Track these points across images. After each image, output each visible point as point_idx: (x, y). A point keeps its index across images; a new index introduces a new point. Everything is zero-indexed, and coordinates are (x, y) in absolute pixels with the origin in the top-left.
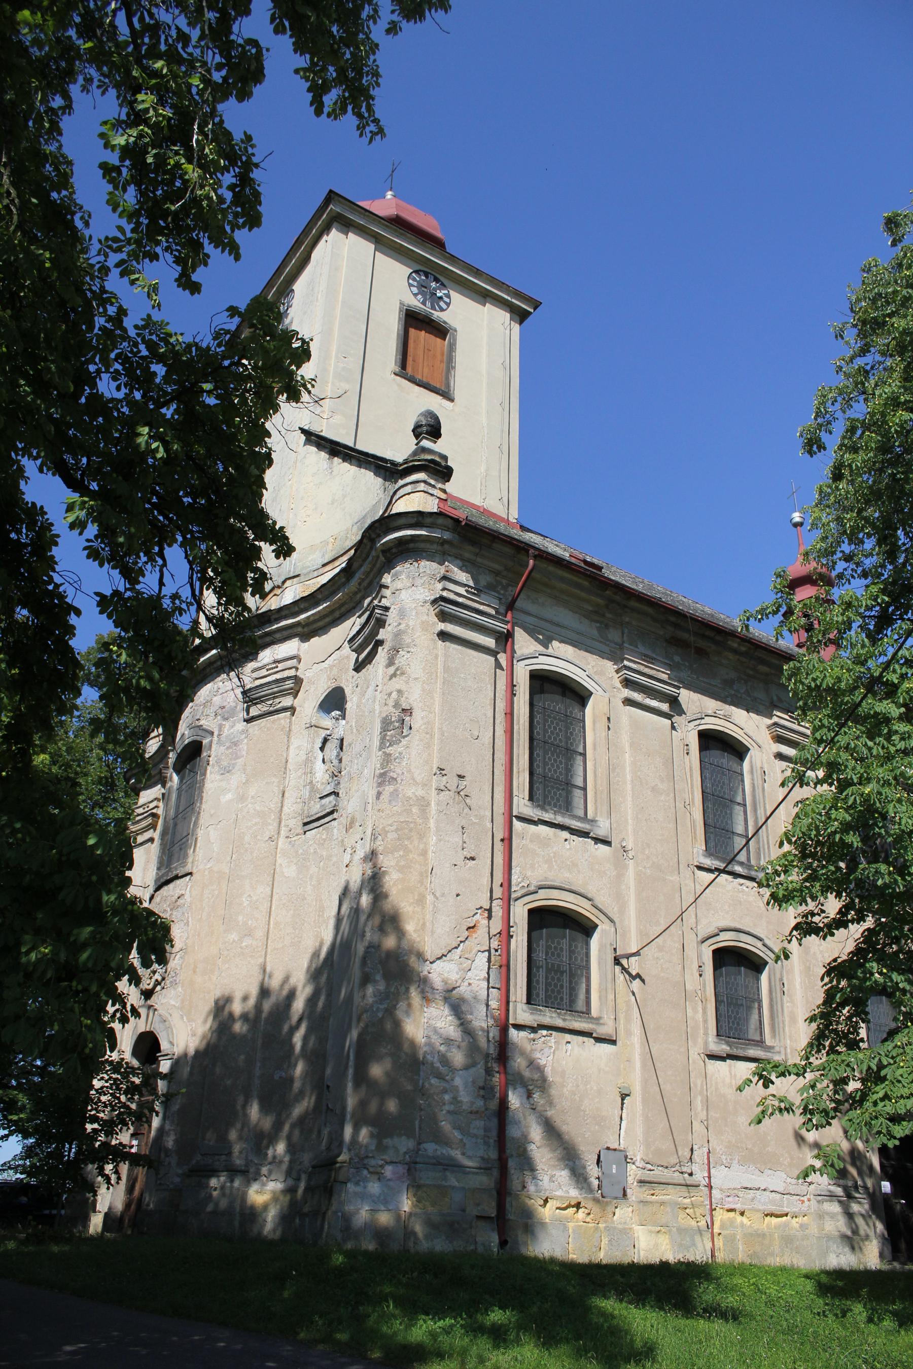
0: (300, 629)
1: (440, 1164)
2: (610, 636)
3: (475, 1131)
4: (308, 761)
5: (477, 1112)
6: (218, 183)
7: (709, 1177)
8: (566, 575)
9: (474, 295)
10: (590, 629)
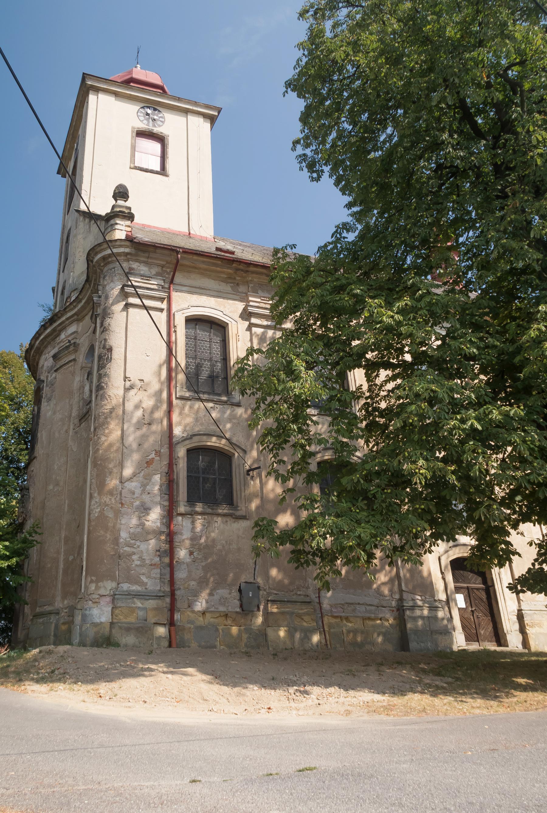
0: (76, 317)
1: (131, 595)
2: (240, 290)
3: (154, 575)
4: (82, 387)
5: (155, 565)
6: (417, 63)
7: (319, 597)
8: (205, 259)
9: (180, 113)
10: (227, 288)
